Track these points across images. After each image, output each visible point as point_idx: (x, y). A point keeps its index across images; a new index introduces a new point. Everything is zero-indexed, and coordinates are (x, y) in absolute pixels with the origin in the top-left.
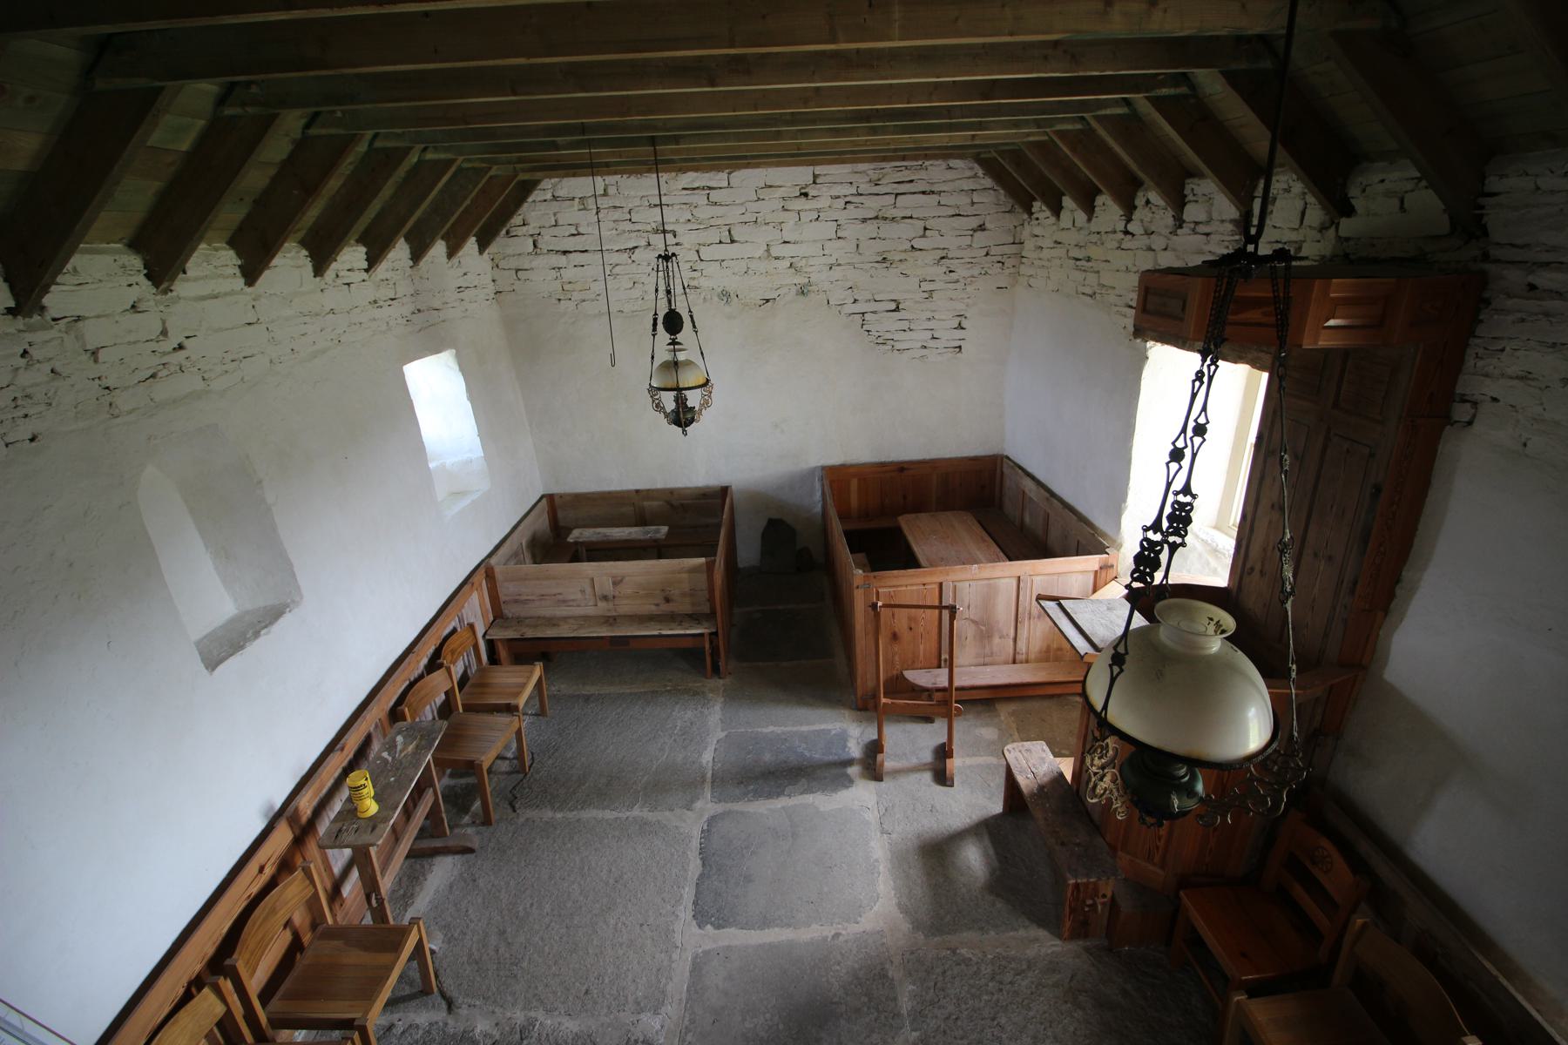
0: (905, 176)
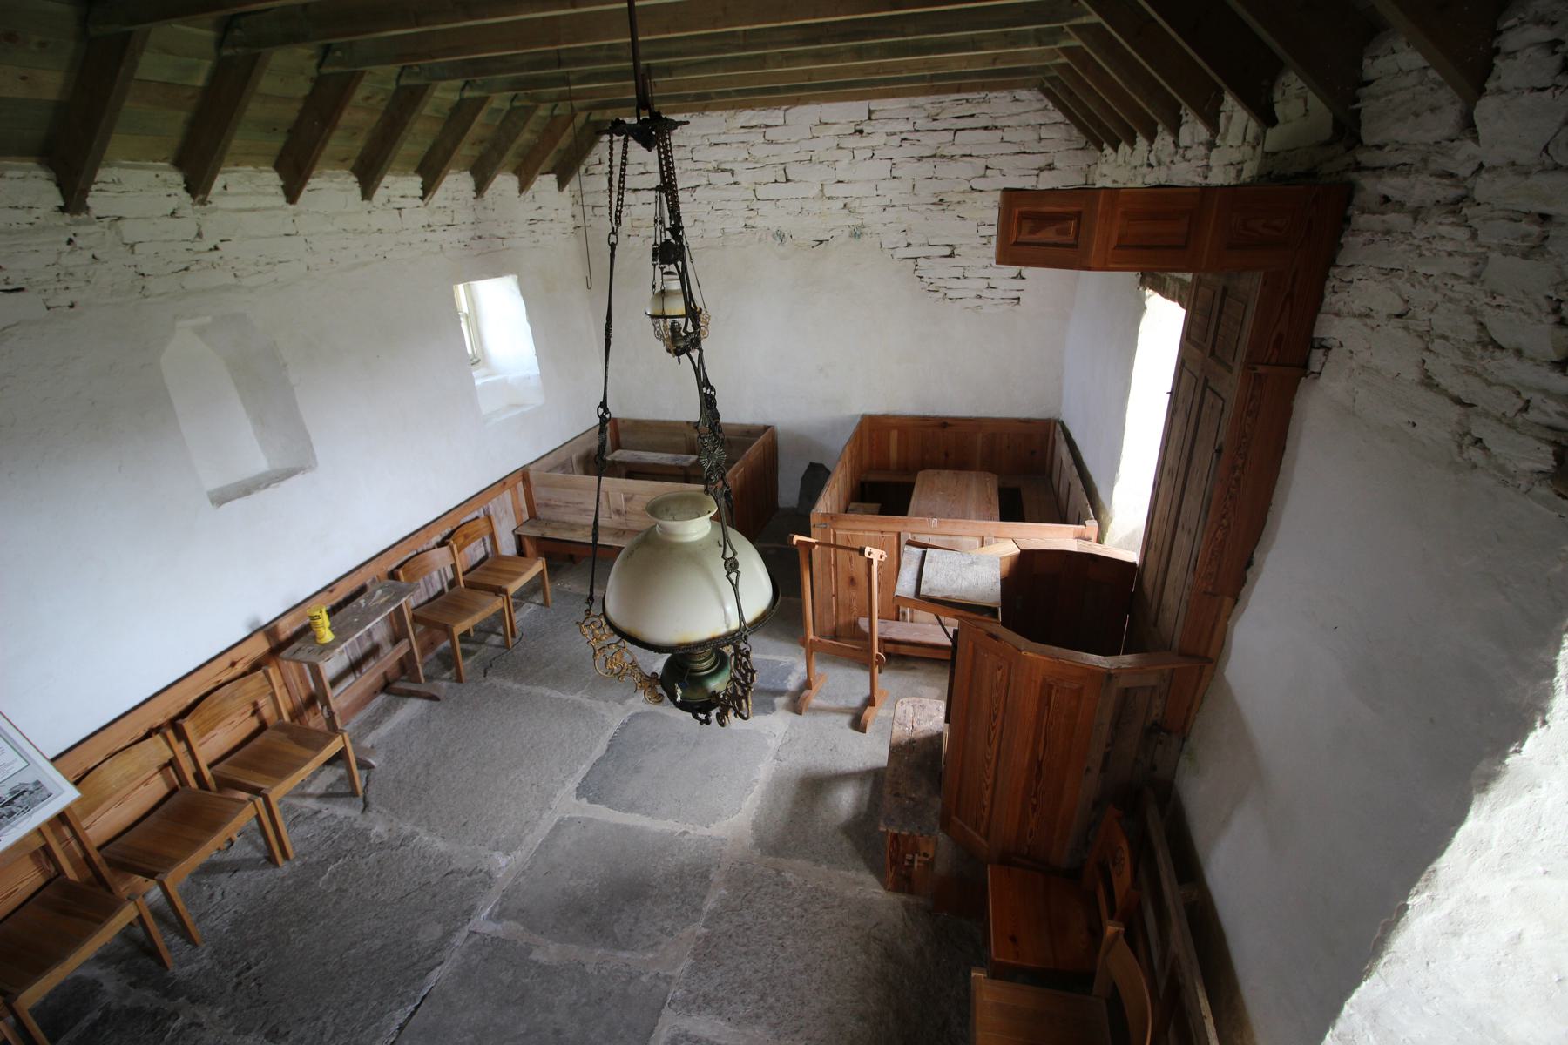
0: (966, 109)
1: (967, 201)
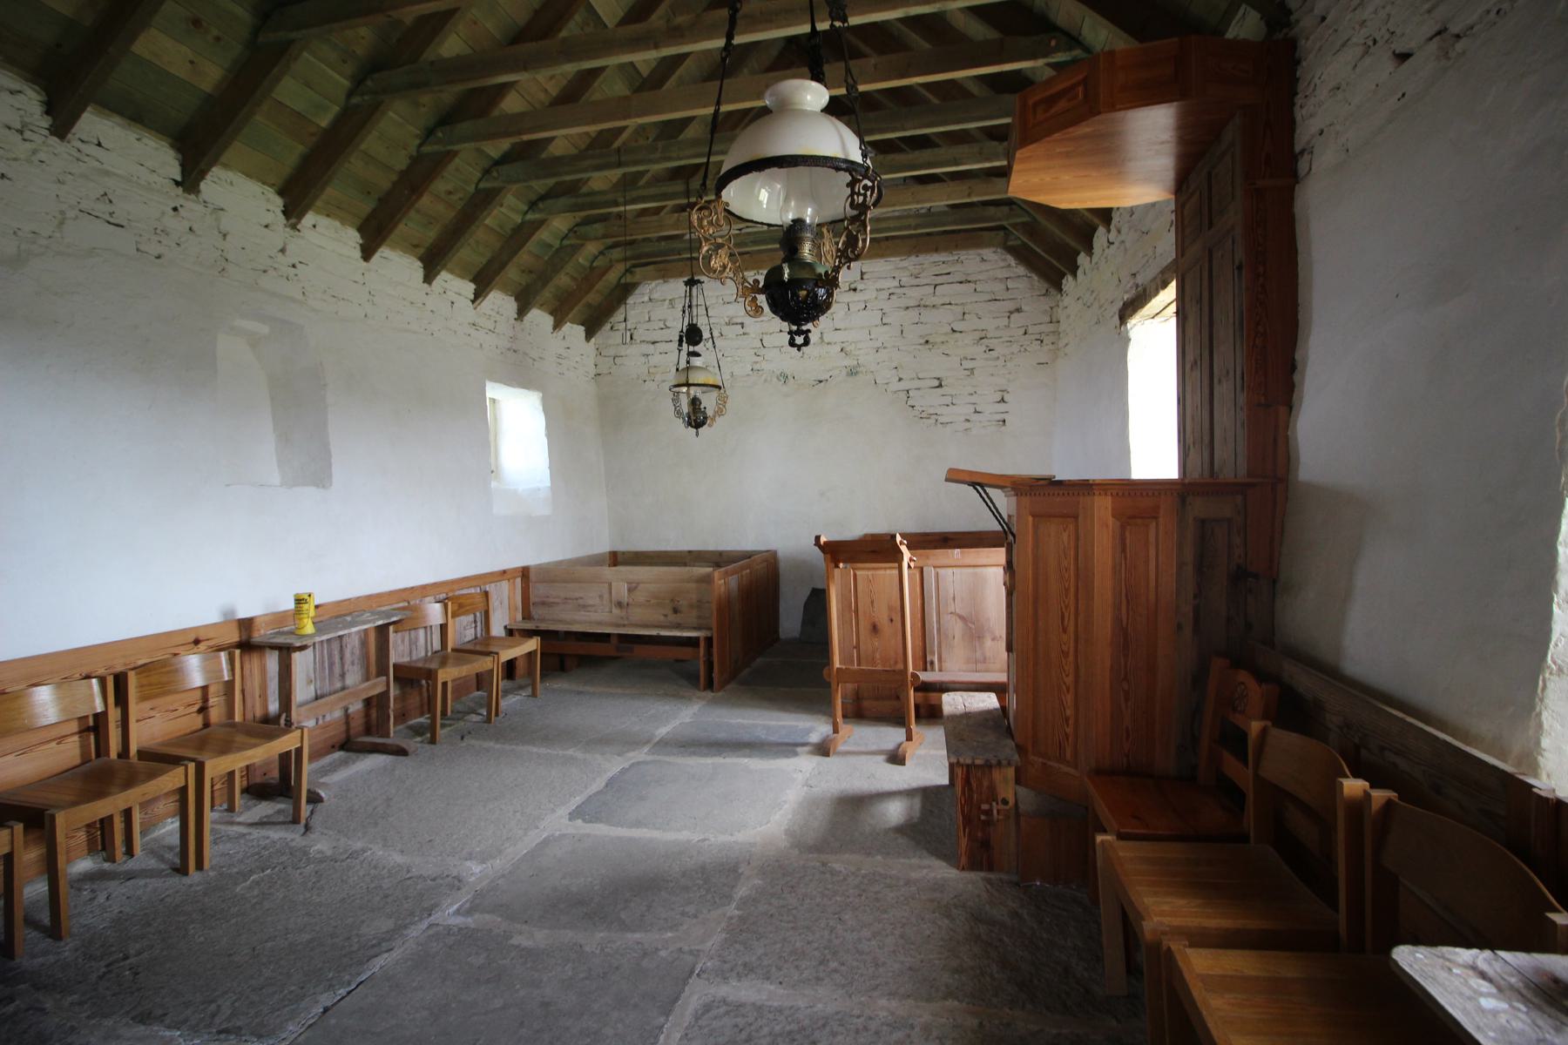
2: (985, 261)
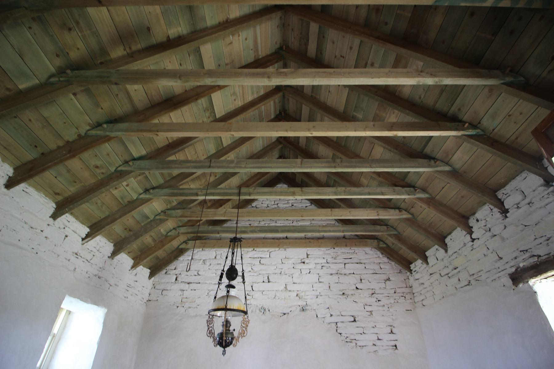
1: (356, 294)
2: (367, 254)
